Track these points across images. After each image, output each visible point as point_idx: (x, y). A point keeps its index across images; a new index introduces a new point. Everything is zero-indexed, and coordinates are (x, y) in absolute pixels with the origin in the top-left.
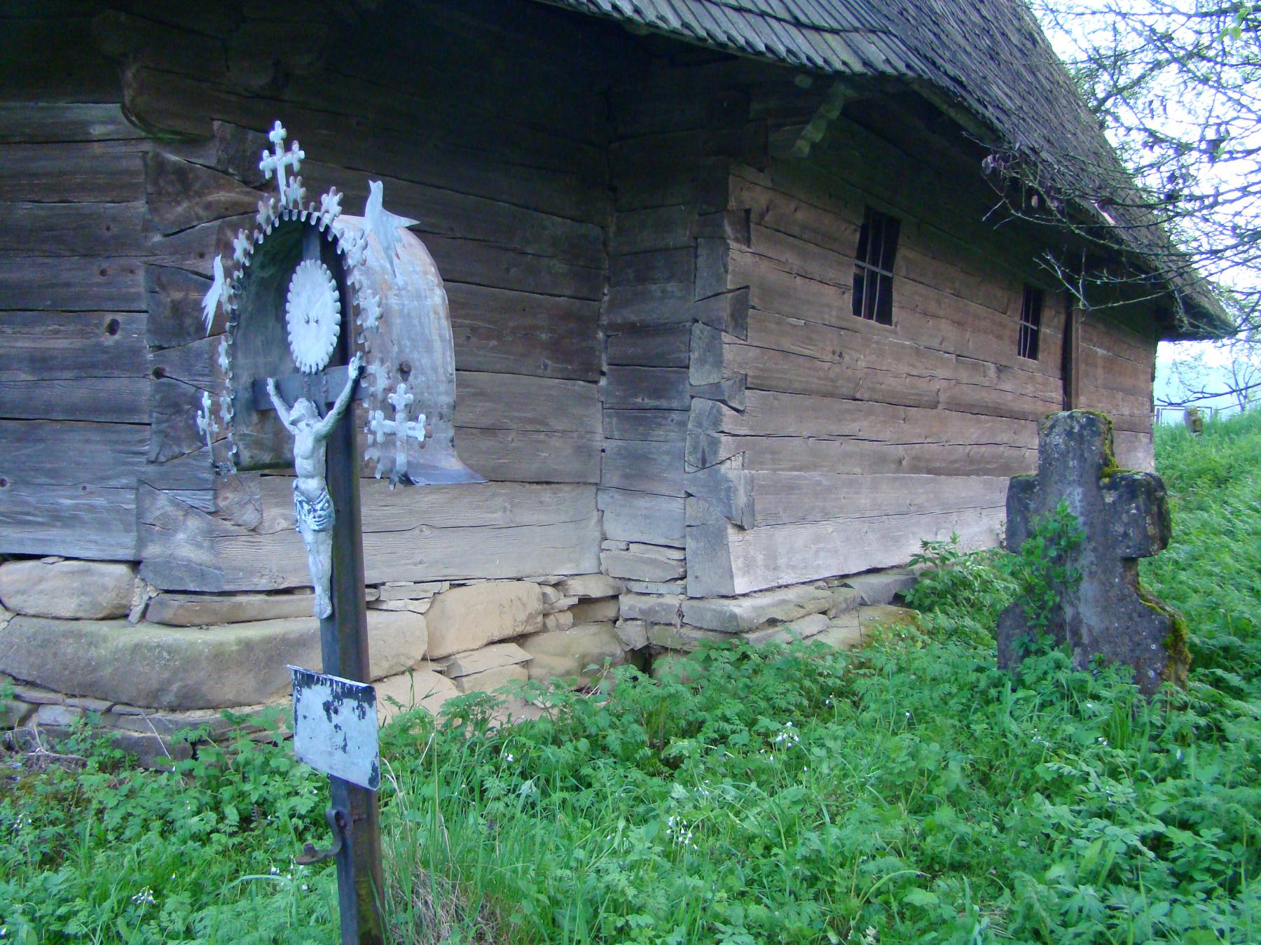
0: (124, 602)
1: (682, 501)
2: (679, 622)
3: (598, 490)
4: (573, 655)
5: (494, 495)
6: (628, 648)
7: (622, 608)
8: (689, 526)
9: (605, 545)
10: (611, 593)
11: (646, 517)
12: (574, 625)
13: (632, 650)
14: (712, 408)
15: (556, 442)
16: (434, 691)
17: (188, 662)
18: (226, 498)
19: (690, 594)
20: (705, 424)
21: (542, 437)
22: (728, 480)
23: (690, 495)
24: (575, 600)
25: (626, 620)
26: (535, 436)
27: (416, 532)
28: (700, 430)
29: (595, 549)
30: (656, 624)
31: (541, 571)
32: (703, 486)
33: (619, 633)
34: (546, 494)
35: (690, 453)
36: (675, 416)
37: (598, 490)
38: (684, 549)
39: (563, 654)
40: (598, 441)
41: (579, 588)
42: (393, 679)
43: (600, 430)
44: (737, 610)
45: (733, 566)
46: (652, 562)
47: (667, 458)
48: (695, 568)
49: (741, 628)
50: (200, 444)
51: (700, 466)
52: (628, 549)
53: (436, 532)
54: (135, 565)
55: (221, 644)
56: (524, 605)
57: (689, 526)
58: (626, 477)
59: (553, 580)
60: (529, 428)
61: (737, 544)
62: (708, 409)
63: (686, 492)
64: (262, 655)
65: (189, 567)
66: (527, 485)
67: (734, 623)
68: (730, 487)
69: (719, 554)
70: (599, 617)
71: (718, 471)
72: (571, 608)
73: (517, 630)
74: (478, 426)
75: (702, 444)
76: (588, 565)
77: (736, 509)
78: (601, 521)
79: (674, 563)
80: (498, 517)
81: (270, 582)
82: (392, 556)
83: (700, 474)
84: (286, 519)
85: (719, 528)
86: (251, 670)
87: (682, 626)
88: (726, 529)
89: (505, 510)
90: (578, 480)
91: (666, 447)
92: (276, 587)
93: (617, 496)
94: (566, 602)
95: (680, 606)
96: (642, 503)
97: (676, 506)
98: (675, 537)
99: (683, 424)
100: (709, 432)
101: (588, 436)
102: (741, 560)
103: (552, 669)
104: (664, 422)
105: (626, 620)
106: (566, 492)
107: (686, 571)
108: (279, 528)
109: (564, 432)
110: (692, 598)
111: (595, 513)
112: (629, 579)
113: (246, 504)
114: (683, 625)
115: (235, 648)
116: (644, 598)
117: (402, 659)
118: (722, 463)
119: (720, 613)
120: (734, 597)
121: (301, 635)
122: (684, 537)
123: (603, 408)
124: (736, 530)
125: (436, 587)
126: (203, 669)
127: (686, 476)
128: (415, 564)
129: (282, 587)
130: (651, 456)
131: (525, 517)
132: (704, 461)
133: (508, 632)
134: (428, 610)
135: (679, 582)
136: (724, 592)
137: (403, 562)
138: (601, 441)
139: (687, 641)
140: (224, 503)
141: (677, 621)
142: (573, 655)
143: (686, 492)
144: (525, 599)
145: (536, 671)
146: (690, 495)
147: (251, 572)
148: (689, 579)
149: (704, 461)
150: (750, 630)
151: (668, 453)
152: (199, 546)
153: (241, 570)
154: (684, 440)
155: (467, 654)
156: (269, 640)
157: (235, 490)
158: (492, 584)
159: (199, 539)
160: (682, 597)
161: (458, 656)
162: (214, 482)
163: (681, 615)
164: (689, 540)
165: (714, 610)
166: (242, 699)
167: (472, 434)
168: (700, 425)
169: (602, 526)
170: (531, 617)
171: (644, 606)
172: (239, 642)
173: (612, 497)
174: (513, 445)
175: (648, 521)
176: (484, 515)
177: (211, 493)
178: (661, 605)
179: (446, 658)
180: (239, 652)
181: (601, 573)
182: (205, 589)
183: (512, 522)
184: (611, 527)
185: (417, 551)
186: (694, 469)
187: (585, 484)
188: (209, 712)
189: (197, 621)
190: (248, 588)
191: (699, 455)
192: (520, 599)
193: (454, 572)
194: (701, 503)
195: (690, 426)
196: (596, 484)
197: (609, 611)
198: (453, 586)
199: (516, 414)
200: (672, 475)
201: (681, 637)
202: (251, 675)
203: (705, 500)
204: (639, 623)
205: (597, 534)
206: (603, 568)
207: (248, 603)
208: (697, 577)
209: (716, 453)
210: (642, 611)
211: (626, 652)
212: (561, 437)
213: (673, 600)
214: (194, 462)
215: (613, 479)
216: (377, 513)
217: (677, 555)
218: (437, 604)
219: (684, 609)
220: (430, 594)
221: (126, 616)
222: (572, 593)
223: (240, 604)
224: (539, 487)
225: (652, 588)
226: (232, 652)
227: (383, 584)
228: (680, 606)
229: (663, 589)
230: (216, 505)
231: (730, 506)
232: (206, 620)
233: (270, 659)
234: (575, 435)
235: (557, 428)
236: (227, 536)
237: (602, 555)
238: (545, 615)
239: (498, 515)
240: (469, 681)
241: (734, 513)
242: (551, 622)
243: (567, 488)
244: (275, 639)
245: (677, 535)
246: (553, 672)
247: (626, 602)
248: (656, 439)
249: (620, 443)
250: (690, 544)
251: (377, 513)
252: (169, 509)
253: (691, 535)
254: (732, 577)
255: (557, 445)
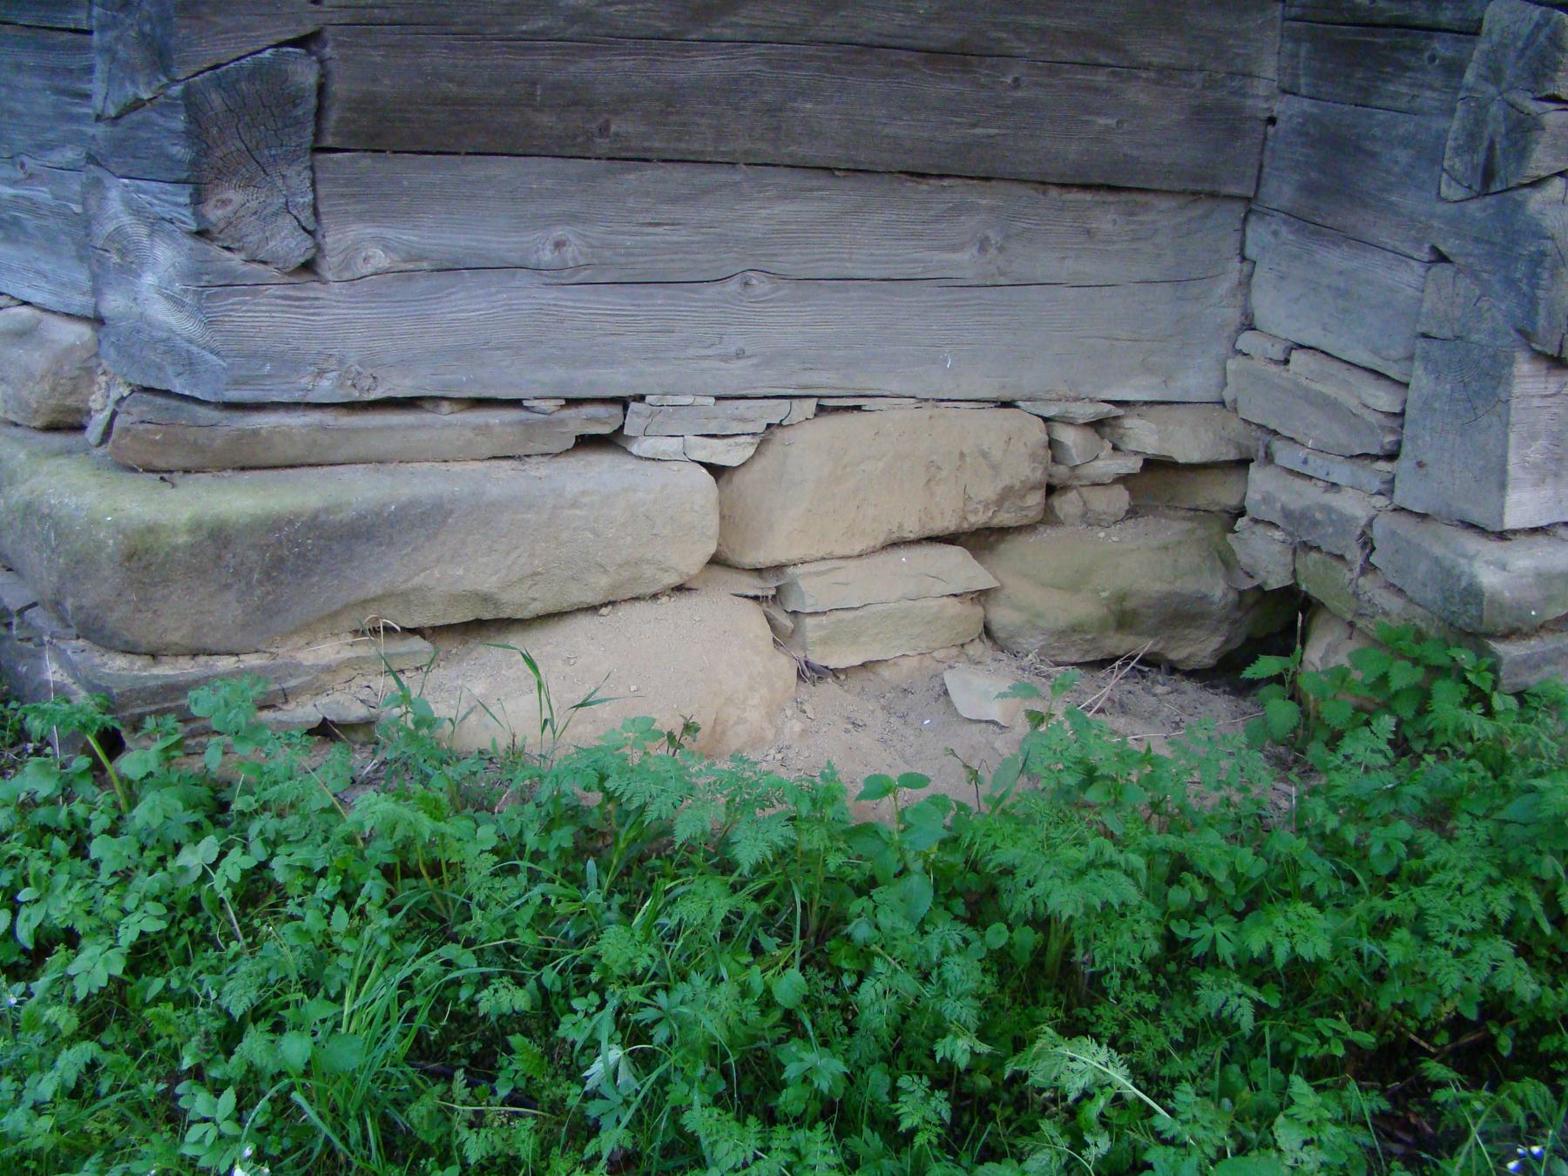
0: (71, 402)
1: (1418, 269)
2: (1359, 561)
3: (1249, 212)
4: (1097, 592)
5: (958, 210)
6: (1247, 584)
7: (1250, 494)
8: (1425, 336)
9: (1246, 341)
10: (1232, 455)
11: (1340, 293)
12: (1132, 513)
13: (1259, 588)
14: (1538, 26)
15: (1138, 94)
16: (599, 695)
17: (77, 562)
18: (225, 203)
19: (1398, 499)
20: (1508, 74)
21: (1100, 78)
22: (1539, 234)
23: (1441, 258)
24: (1133, 465)
25: (1256, 521)
26: (1081, 77)
27: (733, 286)
28: (1492, 90)
29: (1222, 348)
30: (1312, 548)
31: (1063, 389)
32: (1477, 240)
33: (1236, 546)
34: (1107, 218)
35: (1457, 151)
36: (1441, 47)
37: (1249, 212)
38: (1406, 385)
39: (1073, 586)
40: (1262, 96)
41: (1145, 436)
42: (623, 611)
43: (1270, 73)
44: (1489, 579)
45: (1513, 459)
46: (1329, 406)
47: (1403, 156)
48: (1420, 441)
49: (1484, 628)
50: (165, 80)
51: (1476, 187)
52: (1286, 362)
53: (787, 290)
54: (98, 321)
55: (151, 530)
56: (995, 467)
57: (1425, 336)
58: (1310, 189)
59: (1087, 411)
60: (1064, 54)
61: (1536, 402)
62: (1526, 30)
63: (1434, 249)
64: (253, 556)
65: (169, 345)
66: (1054, 193)
67: (1473, 611)
68: (1543, 254)
69: (1484, 422)
70: (1201, 502)
71: (1520, 205)
72: (1123, 479)
73: (972, 519)
74: (922, 43)
75: (1490, 128)
76: (1194, 382)
77: (1551, 314)
78: (1246, 283)
79: (1373, 418)
80: (965, 261)
81: (342, 386)
82: (664, 338)
83: (1473, 206)
84: (387, 248)
85: (1494, 357)
86: (228, 586)
87: (1363, 572)
88: (1510, 361)
89: (983, 245)
90: (1191, 187)
91: (1406, 126)
92: (356, 395)
93: (1285, 233)
94: (1110, 465)
95: (1370, 524)
96: (1335, 258)
97: (1407, 277)
98: (1393, 353)
99: (1454, 69)
100: (1514, 97)
101: (1236, 84)
102: (1541, 443)
103: (1039, 615)
104: (1413, 61)
105: (1256, 521)
106: (1162, 214)
107: (1399, 443)
108: (369, 269)
109: (1161, 70)
110: (1399, 510)
111: (1235, 265)
112: (1275, 433)
113: (275, 214)
114: (1368, 568)
115: (183, 539)
116: (1299, 484)
117: (648, 571)
118: (1537, 183)
119: (1446, 574)
120: (1502, 536)
121: (361, 517)
122: (1411, 358)
123: (1285, 19)
124: (1542, 367)
125: (775, 411)
126: (106, 580)
127: (1440, 208)
128: (725, 358)
129: (372, 396)
130: (1368, 145)
131: (1045, 264)
132: (1488, 174)
133: (947, 522)
134: (753, 456)
135: (1382, 465)
136: (1476, 516)
137: (691, 352)
138: (1267, 99)
139: (1369, 611)
140: (219, 213)
141: (1355, 555)
142: (1097, 592)
143: (1434, 249)
144: (996, 454)
145: (1002, 617)
146: (1441, 258)
147: (290, 363)
148: (1403, 465)
149: (1488, 174)
150: (1510, 634)
151: (1405, 142)
152: (178, 303)
153: (267, 357)
154: (1451, 112)
155: (823, 566)
156: (274, 525)
157: (249, 183)
158: (928, 410)
159: (178, 286)
160: (1381, 501)
161: (801, 569)
162: (194, 164)
163: (1368, 544)
164: (1418, 369)
165: (1436, 560)
166: (209, 642)
167: (899, 63)
168: (1494, 74)
169: (1247, 296)
170: (1006, 495)
171: (1295, 504)
172: (196, 526)
173: (1275, 233)
174: (1019, 94)
175: (1340, 302)
176: (926, 255)
177: (189, 189)
178: (1327, 509)
179: (779, 568)
180: (193, 548)
181: (1222, 403)
182: (197, 394)
183: (1003, 274)
184: (1269, 305)
185: (731, 329)
186: (1460, 193)
187: (1213, 195)
188: (140, 662)
189: (159, 463)
190: (285, 398)
191: (1479, 158)
192: (984, 455)
193: (826, 380)
194: (1464, 283)
195: (1469, 77)
196: (1248, 200)
197: (1223, 494)
198: (821, 410)
199: (1033, 21)
200: (1409, 202)
201: (1356, 595)
202: (230, 596)
203: (1475, 276)
204: (1278, 535)
205: (1233, 315)
206: (1228, 396)
207: (274, 431)
208: (1420, 465)
209: (1522, 155)
210: (1287, 514)
211: (1241, 593)
212: (1157, 82)
213: (1354, 506)
214: (161, 121)
215: (1282, 190)
216: (629, 241)
217: (1385, 400)
218: (773, 450)
219: (1377, 533)
220: (760, 427)
221: (81, 428)
222: (1133, 446)
223: (255, 433)
224: (1088, 196)
225: (1316, 465)
226: (175, 549)
227: (641, 398)
228: (1370, 524)
229: (1342, 472)
230: (198, 215)
231: (1533, 302)
232: (177, 460)
233: (279, 562)
234: (1197, 78)
235: (1147, 57)
236: (230, 283)
237: (1232, 365)
238: (1051, 490)
239: (964, 256)
240: (820, 626)
241: (1542, 322)
242: (1067, 505)
243: (1164, 203)
244: (290, 522)
245: (1398, 352)
246: (1041, 623)
247: (1259, 479)
248: (1388, 103)
249: (1307, 105)
250: (1421, 380)
251: (629, 241)
252: (126, 219)
253: (1426, 358)
254: (1503, 486)
255: (1144, 99)
